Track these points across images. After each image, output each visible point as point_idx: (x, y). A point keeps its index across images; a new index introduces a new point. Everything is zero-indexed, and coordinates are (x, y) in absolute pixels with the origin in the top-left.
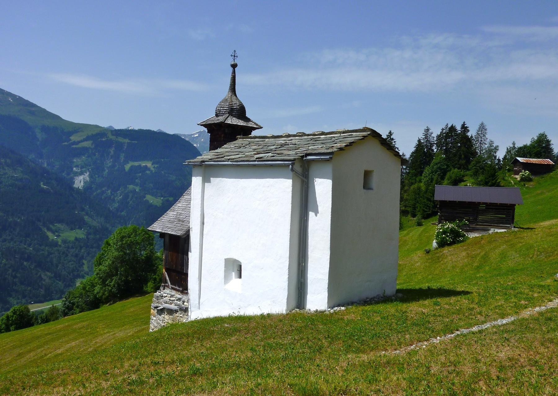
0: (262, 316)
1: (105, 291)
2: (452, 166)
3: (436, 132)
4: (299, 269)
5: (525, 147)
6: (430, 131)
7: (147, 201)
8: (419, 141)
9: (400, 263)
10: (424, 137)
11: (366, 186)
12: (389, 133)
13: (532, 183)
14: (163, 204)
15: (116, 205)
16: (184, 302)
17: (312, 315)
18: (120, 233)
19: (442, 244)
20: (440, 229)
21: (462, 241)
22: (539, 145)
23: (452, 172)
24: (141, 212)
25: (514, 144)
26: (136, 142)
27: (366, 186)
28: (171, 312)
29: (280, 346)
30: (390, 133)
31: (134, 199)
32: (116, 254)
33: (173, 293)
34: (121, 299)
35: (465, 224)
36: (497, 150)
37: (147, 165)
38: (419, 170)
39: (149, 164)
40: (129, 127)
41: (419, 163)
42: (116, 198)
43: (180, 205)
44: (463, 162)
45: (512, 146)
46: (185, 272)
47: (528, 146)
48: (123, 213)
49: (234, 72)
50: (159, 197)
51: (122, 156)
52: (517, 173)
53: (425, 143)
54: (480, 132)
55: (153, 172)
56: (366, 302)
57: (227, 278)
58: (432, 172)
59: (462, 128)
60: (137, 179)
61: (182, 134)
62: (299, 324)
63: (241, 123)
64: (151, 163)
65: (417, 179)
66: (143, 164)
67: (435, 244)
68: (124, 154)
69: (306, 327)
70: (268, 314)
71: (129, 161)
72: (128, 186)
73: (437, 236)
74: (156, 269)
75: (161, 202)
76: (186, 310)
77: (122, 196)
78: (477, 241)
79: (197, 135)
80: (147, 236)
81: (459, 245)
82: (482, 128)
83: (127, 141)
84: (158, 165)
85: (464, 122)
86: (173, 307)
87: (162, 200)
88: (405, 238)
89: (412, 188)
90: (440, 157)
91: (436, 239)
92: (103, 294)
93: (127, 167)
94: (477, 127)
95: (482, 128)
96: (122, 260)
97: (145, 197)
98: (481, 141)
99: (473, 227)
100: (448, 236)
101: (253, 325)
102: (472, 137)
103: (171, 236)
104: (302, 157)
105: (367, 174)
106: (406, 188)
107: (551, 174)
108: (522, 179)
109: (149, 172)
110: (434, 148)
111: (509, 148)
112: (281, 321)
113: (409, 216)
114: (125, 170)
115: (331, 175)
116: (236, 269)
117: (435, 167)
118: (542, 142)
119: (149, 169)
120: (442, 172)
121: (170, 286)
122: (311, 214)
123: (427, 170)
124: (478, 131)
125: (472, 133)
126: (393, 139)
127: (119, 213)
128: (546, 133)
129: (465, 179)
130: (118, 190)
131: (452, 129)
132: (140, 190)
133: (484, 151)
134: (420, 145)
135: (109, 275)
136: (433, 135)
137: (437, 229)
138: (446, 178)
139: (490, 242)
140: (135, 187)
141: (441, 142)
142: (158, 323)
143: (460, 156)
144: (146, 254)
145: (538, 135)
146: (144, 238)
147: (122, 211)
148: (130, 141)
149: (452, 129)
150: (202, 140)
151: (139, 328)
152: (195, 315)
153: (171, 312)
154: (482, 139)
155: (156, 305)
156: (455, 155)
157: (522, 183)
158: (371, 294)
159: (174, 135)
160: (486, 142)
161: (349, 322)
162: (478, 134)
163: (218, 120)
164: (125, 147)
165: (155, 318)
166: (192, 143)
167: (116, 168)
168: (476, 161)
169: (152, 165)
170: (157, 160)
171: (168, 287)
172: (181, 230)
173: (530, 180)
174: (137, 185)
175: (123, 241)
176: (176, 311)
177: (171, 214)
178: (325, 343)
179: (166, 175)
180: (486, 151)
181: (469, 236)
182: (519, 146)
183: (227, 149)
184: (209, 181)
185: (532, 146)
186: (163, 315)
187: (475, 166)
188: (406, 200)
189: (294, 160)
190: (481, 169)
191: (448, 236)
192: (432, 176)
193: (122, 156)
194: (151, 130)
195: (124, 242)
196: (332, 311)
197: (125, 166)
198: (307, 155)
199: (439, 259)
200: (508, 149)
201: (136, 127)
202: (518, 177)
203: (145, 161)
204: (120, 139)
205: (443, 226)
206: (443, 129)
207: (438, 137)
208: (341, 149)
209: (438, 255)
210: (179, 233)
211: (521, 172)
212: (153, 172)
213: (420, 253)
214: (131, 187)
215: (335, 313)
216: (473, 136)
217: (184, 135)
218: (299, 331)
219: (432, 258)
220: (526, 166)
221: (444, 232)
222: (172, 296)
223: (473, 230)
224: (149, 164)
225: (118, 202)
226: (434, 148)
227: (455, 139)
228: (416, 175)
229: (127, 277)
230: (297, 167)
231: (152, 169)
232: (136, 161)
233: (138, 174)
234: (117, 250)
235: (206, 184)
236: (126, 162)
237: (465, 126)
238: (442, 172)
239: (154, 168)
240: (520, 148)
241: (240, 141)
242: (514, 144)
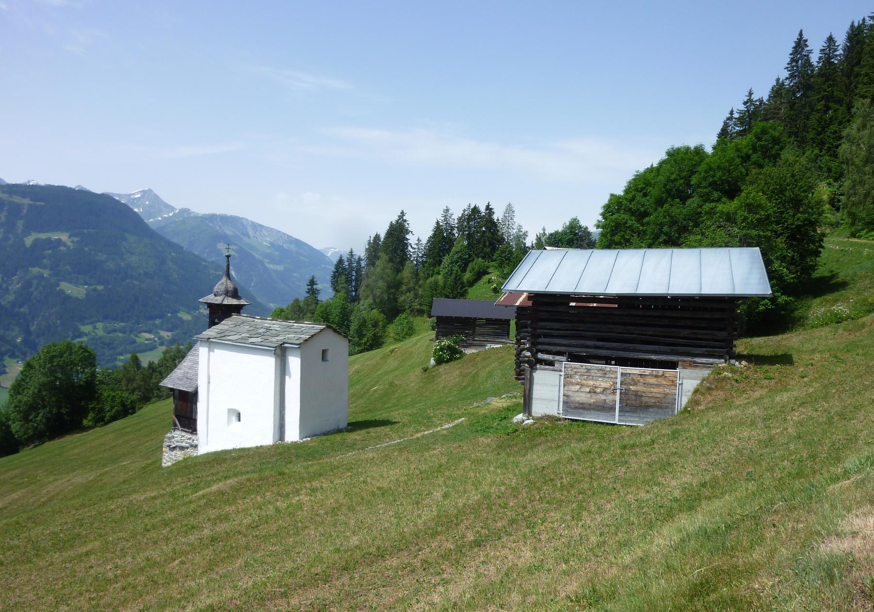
0: (257, 448)
1: (28, 429)
2: (476, 254)
3: (456, 214)
4: (280, 416)
5: (557, 233)
6: (450, 212)
7: (62, 291)
8: (438, 223)
9: (397, 383)
10: (443, 218)
11: (324, 358)
12: (401, 213)
14: (87, 295)
15: (11, 297)
16: (193, 440)
17: (289, 444)
18: (48, 352)
19: (440, 361)
20: (438, 345)
21: (459, 358)
22: (571, 232)
23: (474, 262)
24: (52, 309)
25: (544, 230)
26: (43, 204)
27: (324, 358)
28: (182, 448)
29: (269, 462)
30: (402, 213)
31: (41, 288)
32: (44, 379)
33: (183, 434)
34: (51, 438)
35: (462, 340)
36: (527, 236)
37: (61, 237)
38: (438, 258)
39: (64, 237)
40: (29, 181)
41: (437, 251)
42: (10, 288)
43: (186, 364)
44: (488, 250)
45: (542, 232)
48: (22, 310)
49: (228, 261)
50: (81, 285)
51: (20, 224)
53: (445, 226)
54: (507, 215)
55: (71, 247)
56: (325, 434)
57: (229, 421)
58: (452, 263)
59: (486, 210)
60: (45, 258)
61: (117, 194)
62: (281, 450)
63: (235, 302)
64: (68, 234)
65: (436, 270)
66: (55, 236)
67: (432, 362)
68: (22, 222)
69: (284, 452)
70: (261, 446)
71: (31, 232)
72: (30, 269)
73: (435, 353)
74: (99, 397)
75: (85, 292)
76: (196, 446)
77: (20, 284)
79: (139, 195)
80: (87, 354)
81: (455, 362)
82: (509, 210)
83: (27, 201)
84: (78, 239)
85: (489, 203)
86: (184, 444)
87: (86, 289)
88: (411, 350)
89: (428, 281)
90: (461, 243)
91: (434, 356)
92: (25, 433)
93: (29, 241)
94: (504, 209)
95: (509, 210)
96: (50, 387)
97: (58, 285)
98: (509, 224)
99: (469, 343)
100: (445, 353)
101: (251, 453)
102: (498, 220)
103: (180, 391)
104: (281, 344)
105: (324, 352)
106: (421, 282)
109: (65, 248)
110: (455, 232)
111: (538, 235)
112: (269, 449)
113: (425, 316)
114: (24, 245)
115: (300, 356)
116: (236, 415)
117: (456, 256)
118: (575, 228)
119: (65, 245)
120: (464, 263)
121: (180, 428)
122: (287, 377)
123: (446, 260)
124: (505, 213)
125: (498, 216)
126: (405, 221)
127: (16, 310)
128: (579, 218)
129: (490, 270)
130: (13, 275)
131: (475, 210)
132: (50, 275)
133: (512, 237)
134: (438, 229)
135: (32, 408)
136: (453, 217)
137: (435, 346)
138: (468, 269)
139: (484, 359)
140: (42, 271)
141: (462, 225)
142: (170, 458)
143: (485, 242)
144: (86, 378)
146: (82, 358)
147: (20, 307)
148: (32, 202)
149: (475, 210)
150: (147, 203)
151: (99, 472)
152: (203, 450)
153: (182, 448)
154: (510, 223)
155: (168, 444)
156: (479, 242)
158: (328, 429)
159: (103, 195)
160: (514, 227)
161: (311, 447)
162: (505, 216)
163: (216, 300)
164: (25, 211)
165: (167, 455)
166: (131, 207)
167: (10, 242)
168: (501, 251)
169: (69, 238)
170: (77, 230)
171: (178, 429)
172: (191, 387)
174: (45, 267)
175: (53, 362)
176: (187, 448)
177: (177, 373)
178: (294, 459)
179: (92, 253)
180: (514, 237)
181: (466, 352)
182: (550, 233)
183: (226, 325)
184: (213, 351)
185: (564, 233)
186: (175, 452)
187: (500, 256)
188: (422, 296)
189: (276, 347)
190: (506, 260)
191: (445, 353)
192: (452, 267)
193: (20, 224)
194: (66, 187)
195: (55, 364)
196: (302, 441)
197: (25, 239)
198: (284, 343)
199: (433, 378)
200: (537, 236)
201: (42, 182)
203: (57, 231)
204: (16, 199)
205: (441, 342)
206: (464, 211)
207: (460, 219)
208: (306, 340)
209: (433, 374)
210: (190, 390)
212: (71, 247)
213: (418, 370)
214: (35, 270)
215: (304, 442)
216: (500, 219)
217: (119, 195)
218: (280, 454)
219: (427, 377)
221: (442, 349)
222: (183, 436)
223: (470, 346)
224: (64, 237)
225: (15, 293)
226: (455, 232)
227: (479, 223)
228: (434, 265)
229: (60, 407)
230: (279, 351)
231: (69, 244)
232: (44, 232)
233: (48, 252)
234: (45, 374)
235: (211, 353)
236: (27, 232)
237: (490, 207)
238: (464, 263)
239: (72, 242)
240: (551, 235)
241: (235, 317)
242: (544, 230)
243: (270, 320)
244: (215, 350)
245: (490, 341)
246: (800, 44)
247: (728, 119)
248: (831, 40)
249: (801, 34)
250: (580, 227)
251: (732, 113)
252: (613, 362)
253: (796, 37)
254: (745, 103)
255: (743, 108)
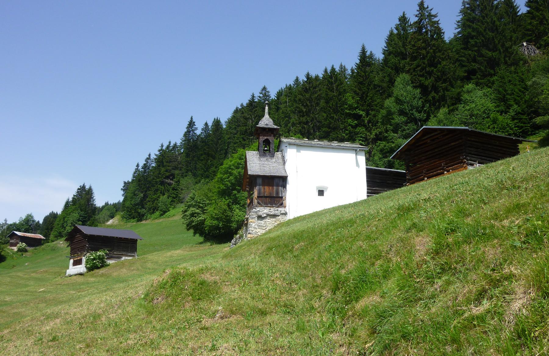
13: (28, 253)
25: (6, 220)
45: (4, 222)
46: (280, 196)
47: (17, 224)
52: (15, 245)
78: (115, 266)
107: (43, 246)
108: (20, 250)
128: (33, 214)
145: (26, 215)
152: (291, 216)
157: (20, 253)
173: (26, 251)
176: (278, 216)
202: (15, 249)
211: (18, 243)
220: (23, 239)
242: (6, 220)
243: (317, 141)
244: (301, 151)
245: (124, 255)
246: (191, 124)
247: (148, 159)
248: (206, 124)
249: (192, 118)
250: (34, 221)
251: (149, 155)
252: (426, 179)
253: (189, 119)
254: (159, 151)
255: (158, 153)
